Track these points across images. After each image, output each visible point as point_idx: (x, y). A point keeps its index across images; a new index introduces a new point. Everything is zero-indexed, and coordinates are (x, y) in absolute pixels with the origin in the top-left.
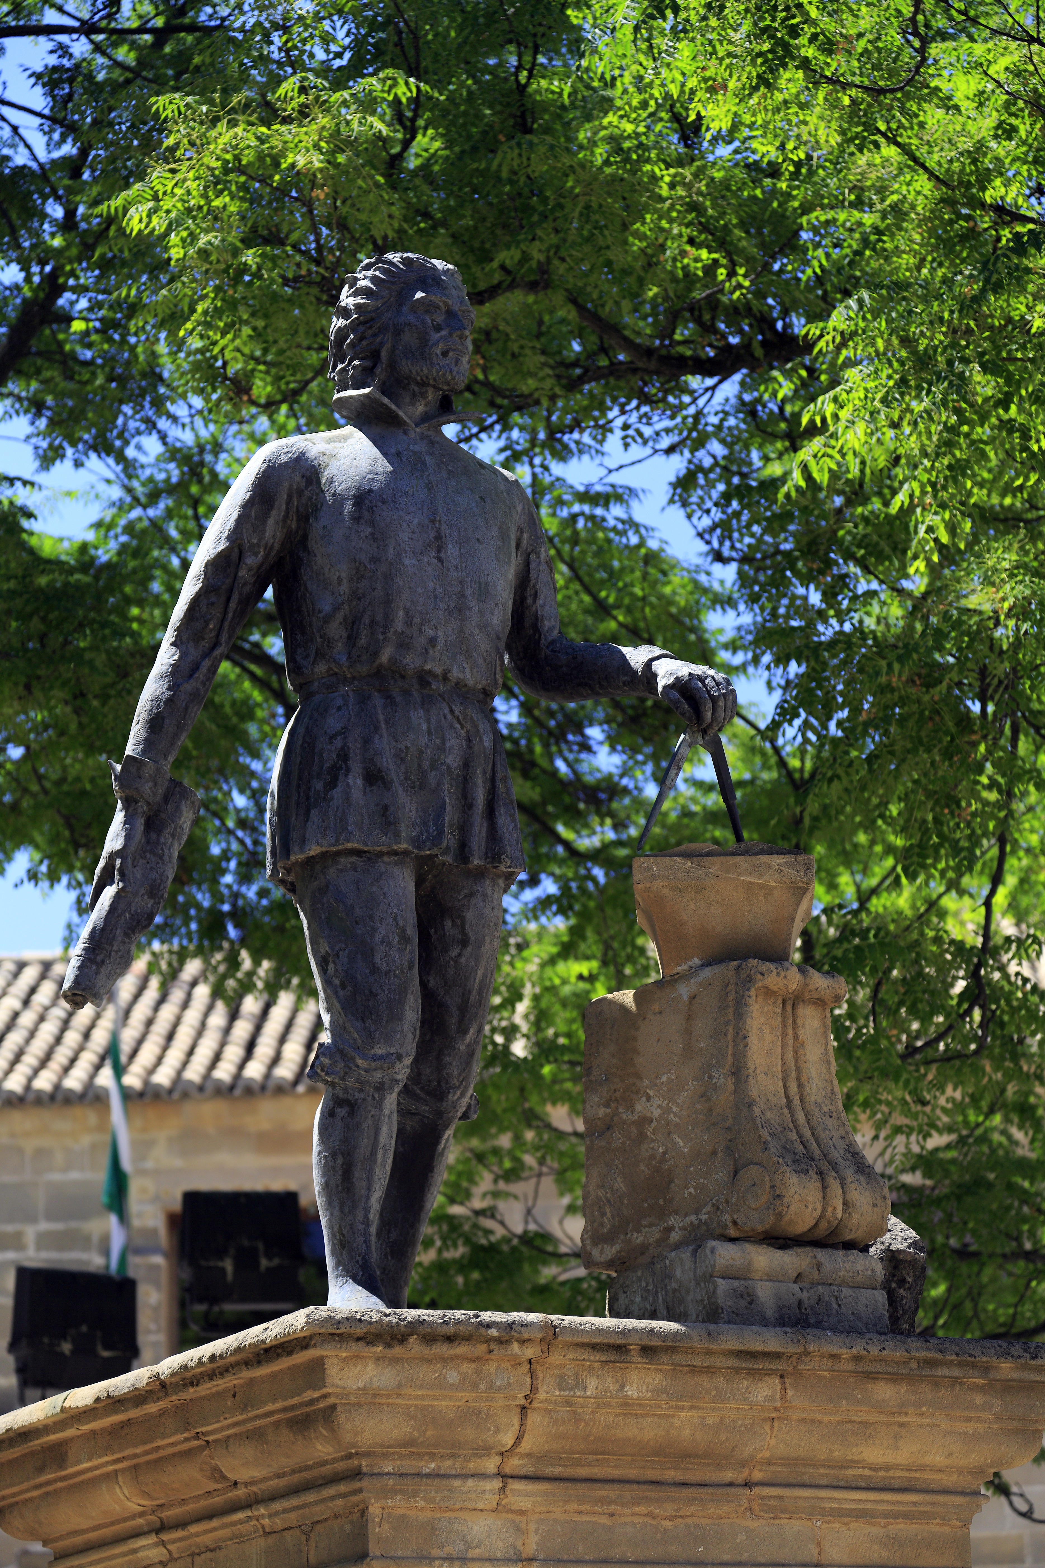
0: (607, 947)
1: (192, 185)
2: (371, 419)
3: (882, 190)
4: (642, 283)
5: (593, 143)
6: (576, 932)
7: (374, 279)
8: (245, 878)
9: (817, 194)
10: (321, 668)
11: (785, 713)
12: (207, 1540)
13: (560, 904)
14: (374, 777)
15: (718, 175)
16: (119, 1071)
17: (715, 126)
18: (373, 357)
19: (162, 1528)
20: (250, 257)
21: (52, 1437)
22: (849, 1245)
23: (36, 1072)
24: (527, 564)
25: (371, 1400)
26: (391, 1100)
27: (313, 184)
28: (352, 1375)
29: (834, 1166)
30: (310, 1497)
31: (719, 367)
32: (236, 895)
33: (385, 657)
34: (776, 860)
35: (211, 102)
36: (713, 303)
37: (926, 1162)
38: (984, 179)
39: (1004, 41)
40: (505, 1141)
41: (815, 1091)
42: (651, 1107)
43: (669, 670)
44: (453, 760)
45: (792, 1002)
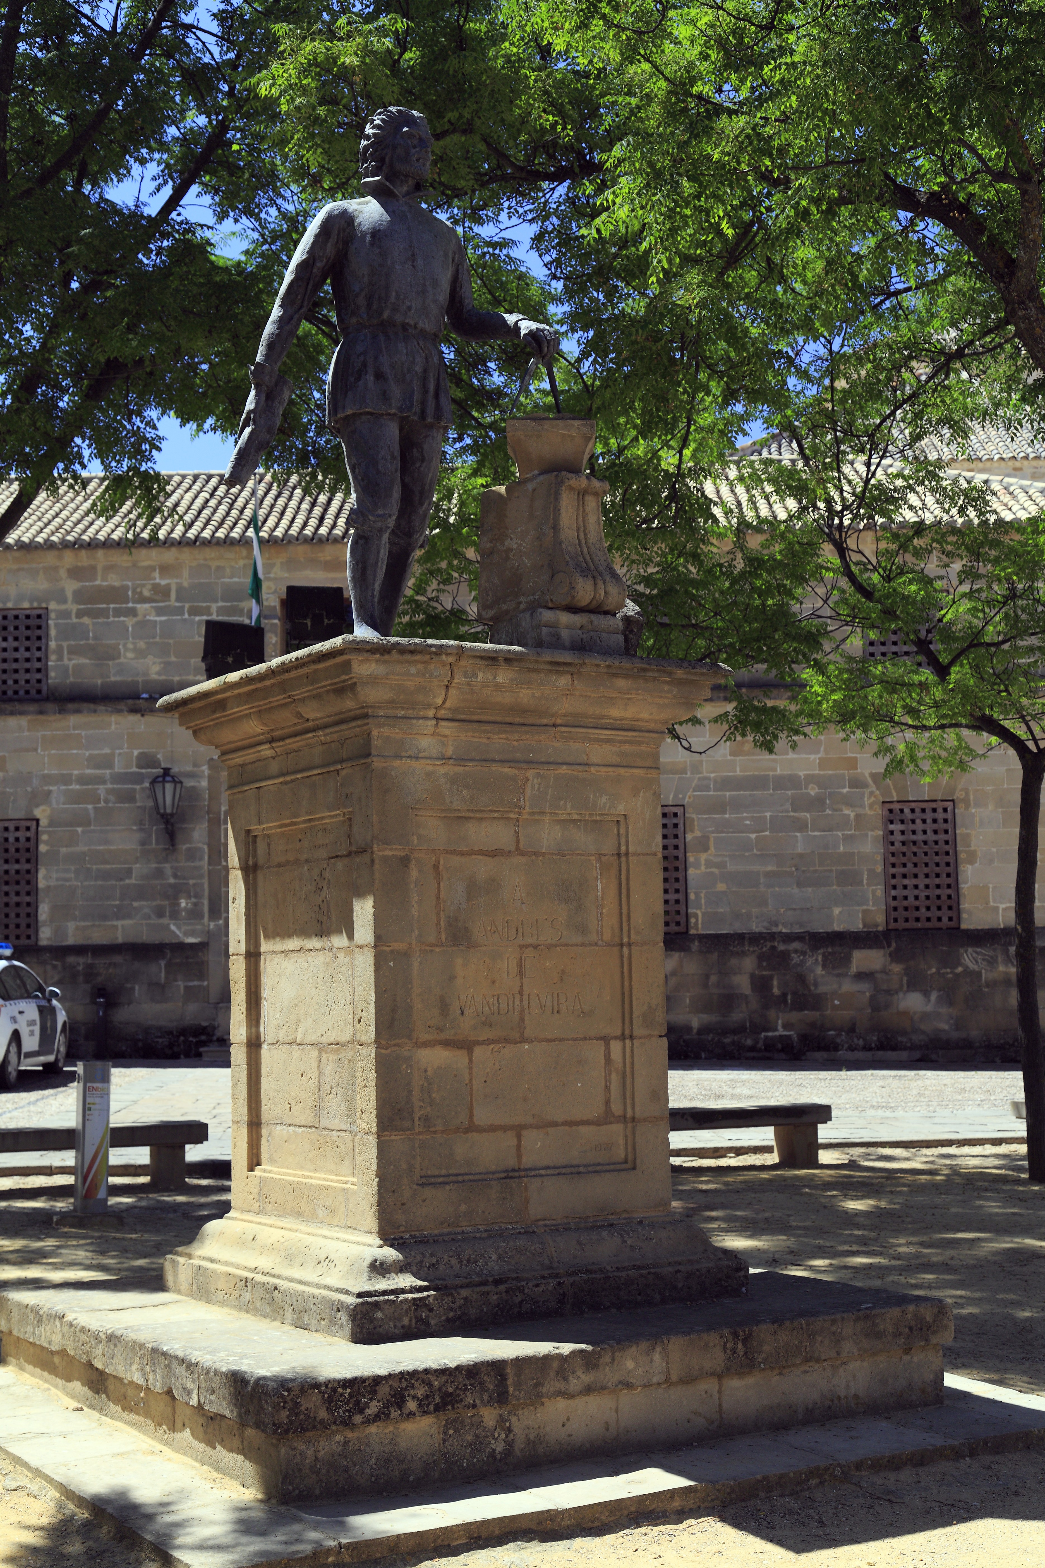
0: (496, 472)
1: (292, 72)
2: (379, 193)
3: (641, 87)
4: (519, 133)
5: (496, 57)
6: (481, 464)
7: (382, 120)
8: (319, 433)
9: (609, 88)
10: (354, 320)
11: (585, 354)
12: (294, 746)
13: (474, 449)
14: (379, 376)
15: (559, 76)
16: (257, 530)
17: (558, 48)
18: (381, 161)
19: (272, 740)
20: (321, 111)
21: (220, 696)
22: (606, 613)
23: (217, 529)
24: (457, 271)
25: (373, 680)
26: (386, 537)
27: (354, 73)
28: (364, 668)
29: (601, 574)
30: (344, 727)
31: (557, 177)
32: (315, 442)
33: (385, 315)
34: (577, 423)
35: (302, 28)
36: (554, 143)
37: (648, 580)
38: (693, 81)
39: (705, 8)
40: (444, 565)
41: (592, 537)
42: (513, 543)
43: (527, 326)
44: (418, 369)
45: (582, 494)
